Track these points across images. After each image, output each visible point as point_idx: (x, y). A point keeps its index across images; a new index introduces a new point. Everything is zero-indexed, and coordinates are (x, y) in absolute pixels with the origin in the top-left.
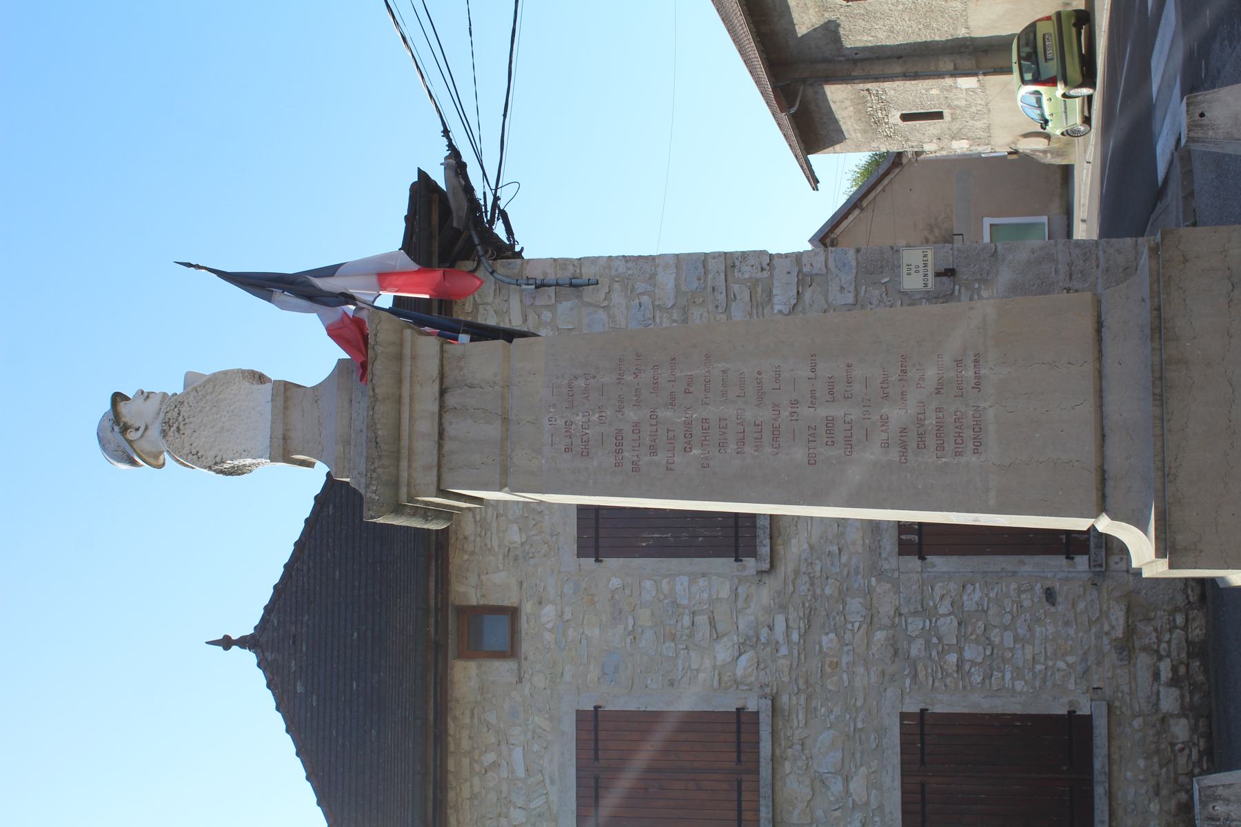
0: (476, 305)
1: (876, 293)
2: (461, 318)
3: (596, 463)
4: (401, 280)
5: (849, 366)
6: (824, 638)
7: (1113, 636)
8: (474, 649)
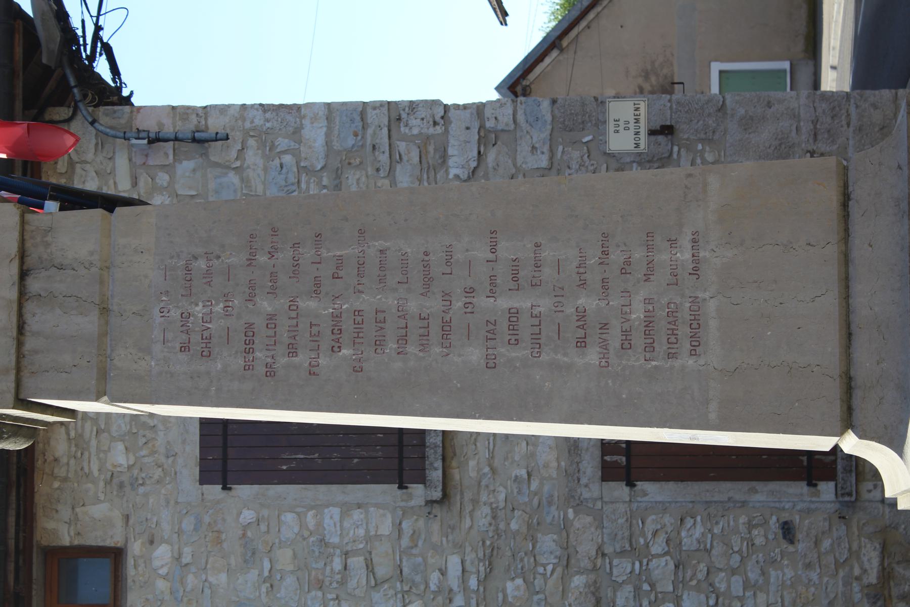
0: (72, 164)
1: (576, 154)
2: (53, 180)
3: (219, 366)
5: (537, 245)
6: (510, 586)
7: (865, 581)
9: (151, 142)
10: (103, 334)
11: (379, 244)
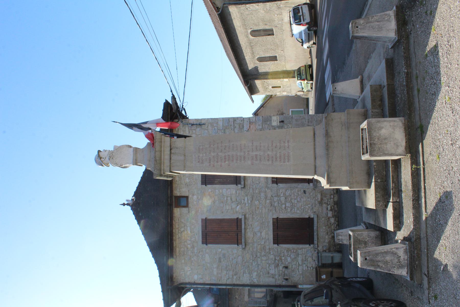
0: (178, 129)
4: (161, 125)
6: (256, 202)
8: (178, 206)
9: (192, 125)
10: (184, 160)
11: (232, 143)
